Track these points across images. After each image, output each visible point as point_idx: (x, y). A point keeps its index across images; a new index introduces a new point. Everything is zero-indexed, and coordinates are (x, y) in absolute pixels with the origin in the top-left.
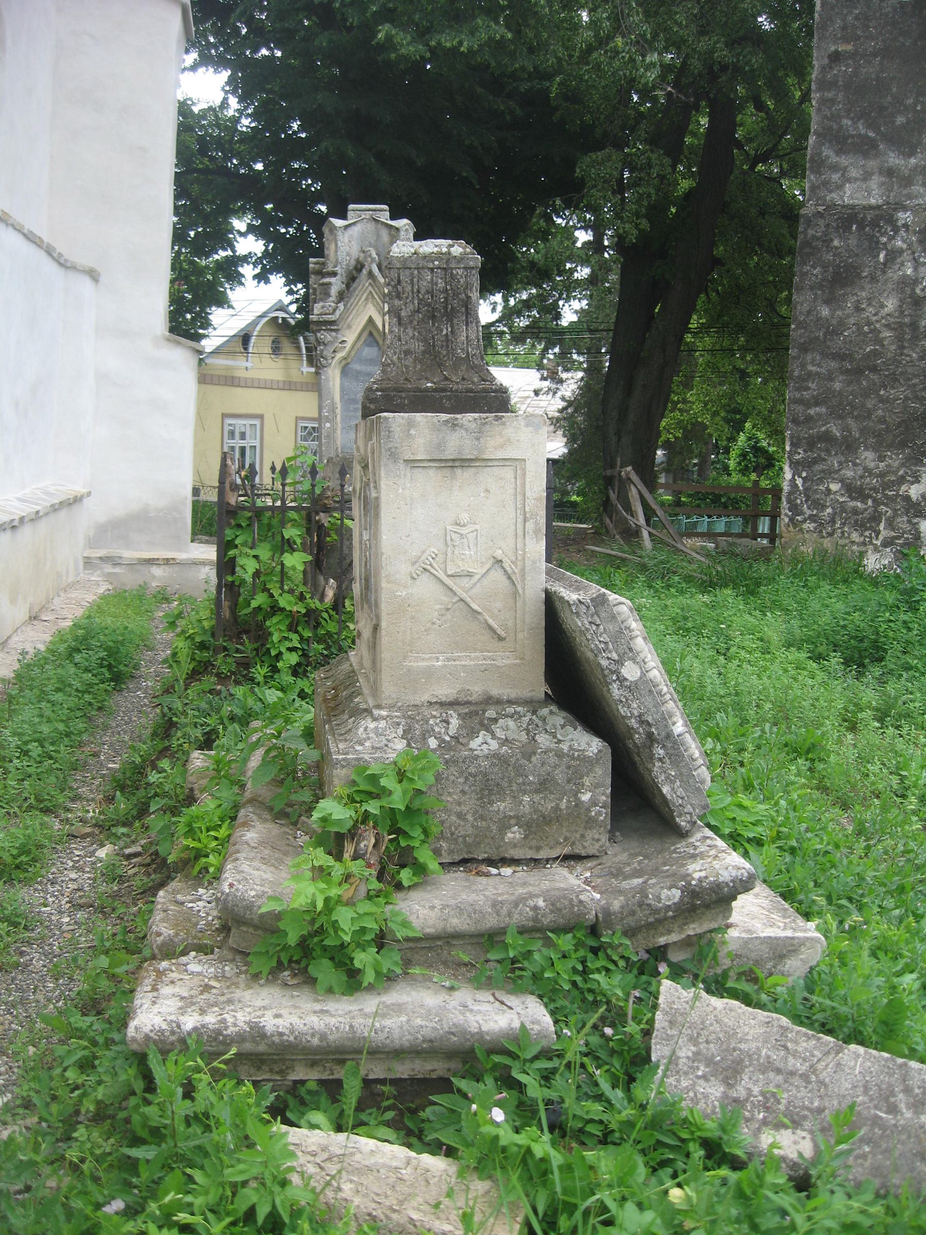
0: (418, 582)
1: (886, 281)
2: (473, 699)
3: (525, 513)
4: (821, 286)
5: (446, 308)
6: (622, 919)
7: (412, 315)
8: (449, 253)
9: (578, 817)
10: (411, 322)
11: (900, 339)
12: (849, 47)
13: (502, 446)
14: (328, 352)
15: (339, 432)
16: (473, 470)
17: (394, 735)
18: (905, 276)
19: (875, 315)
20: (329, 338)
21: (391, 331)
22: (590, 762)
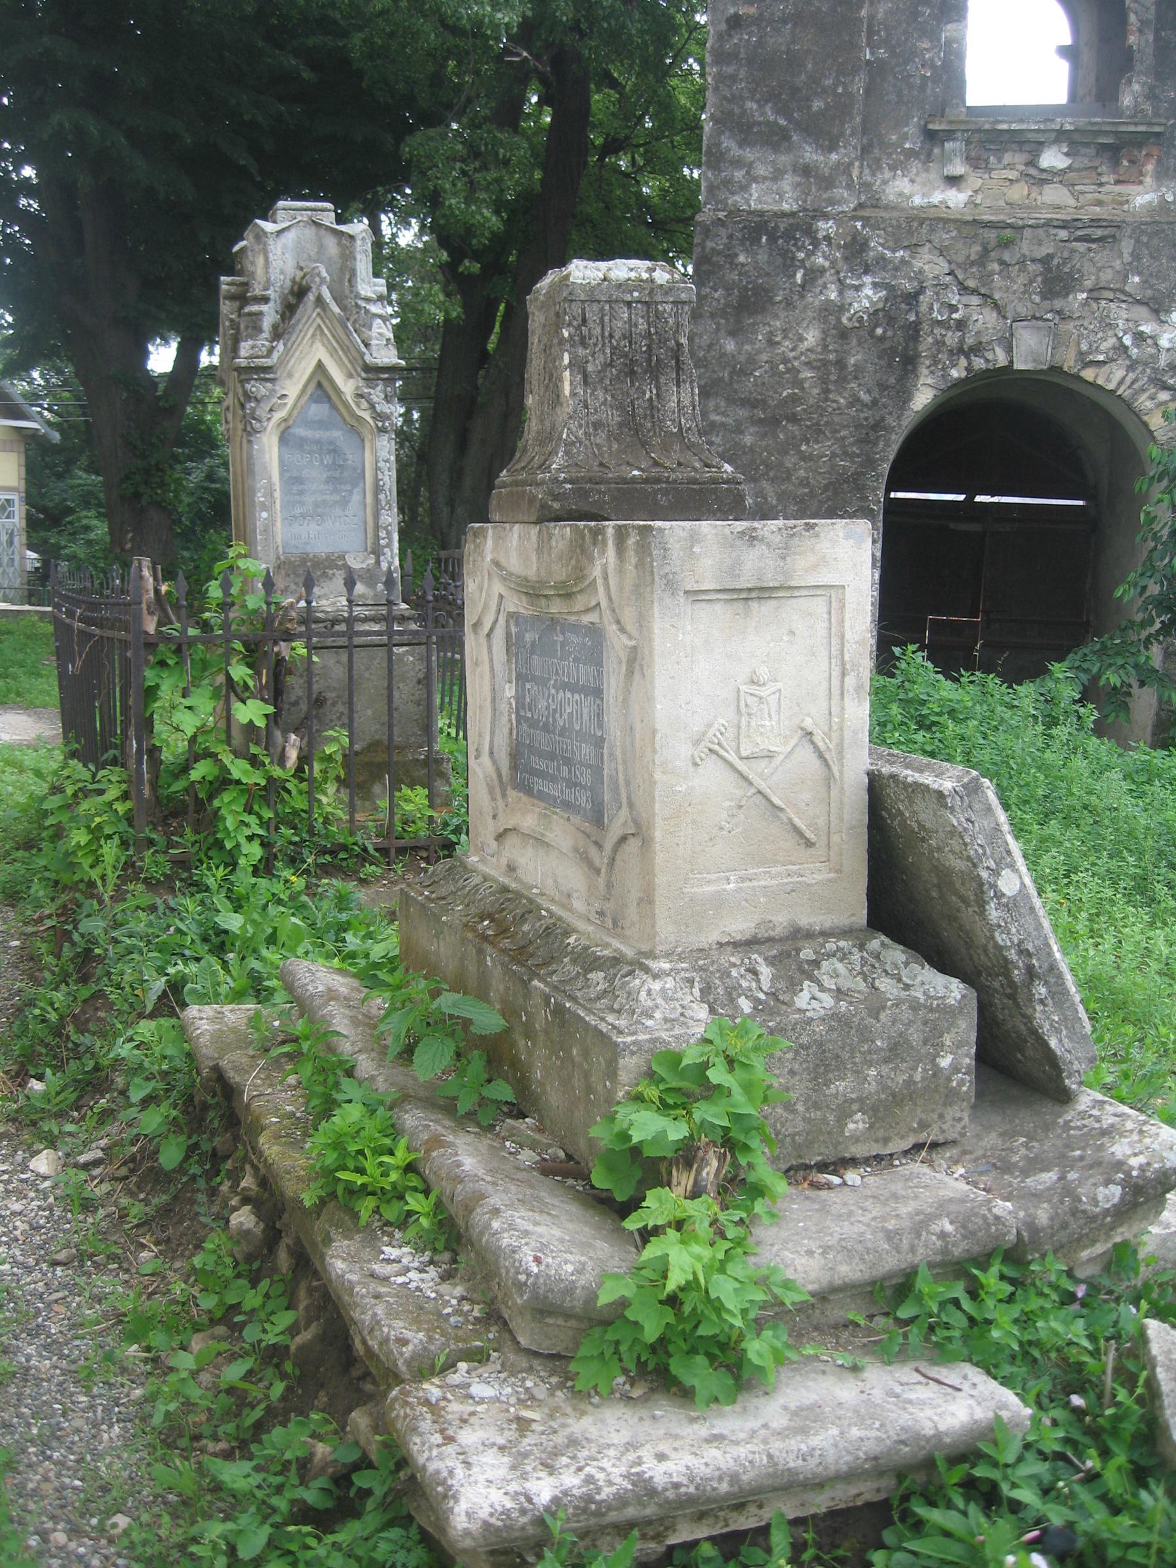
0: (701, 770)
1: (805, 307)
2: (778, 932)
3: (843, 664)
4: (723, 313)
5: (649, 360)
6: (1053, 1235)
7: (603, 370)
8: (652, 281)
9: (936, 1091)
10: (601, 380)
11: (824, 380)
12: (752, 10)
13: (814, 568)
14: (262, 412)
15: (279, 524)
16: (773, 603)
17: (690, 998)
18: (828, 301)
19: (792, 350)
20: (263, 391)
21: (573, 394)
22: (950, 1013)
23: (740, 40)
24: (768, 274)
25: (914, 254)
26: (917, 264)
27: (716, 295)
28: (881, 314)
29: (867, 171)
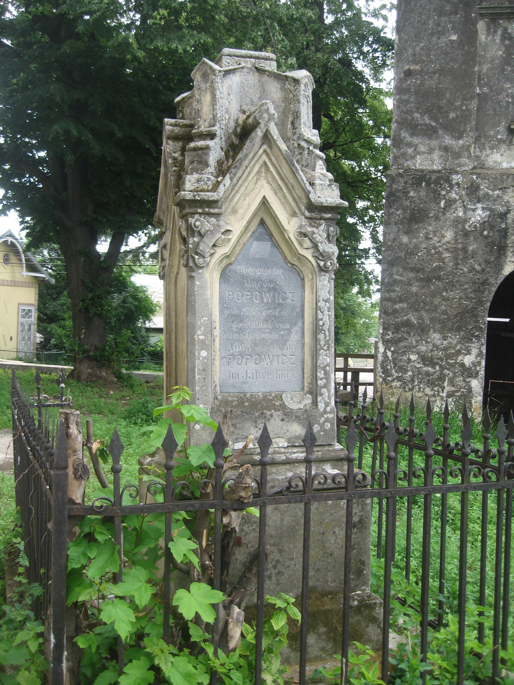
1: (446, 220)
4: (402, 223)
14: (205, 247)
15: (217, 363)
18: (458, 217)
19: (439, 242)
23: (411, 82)
24: (425, 202)
25: (504, 193)
26: (506, 198)
27: (398, 213)
28: (487, 224)
29: (478, 150)
